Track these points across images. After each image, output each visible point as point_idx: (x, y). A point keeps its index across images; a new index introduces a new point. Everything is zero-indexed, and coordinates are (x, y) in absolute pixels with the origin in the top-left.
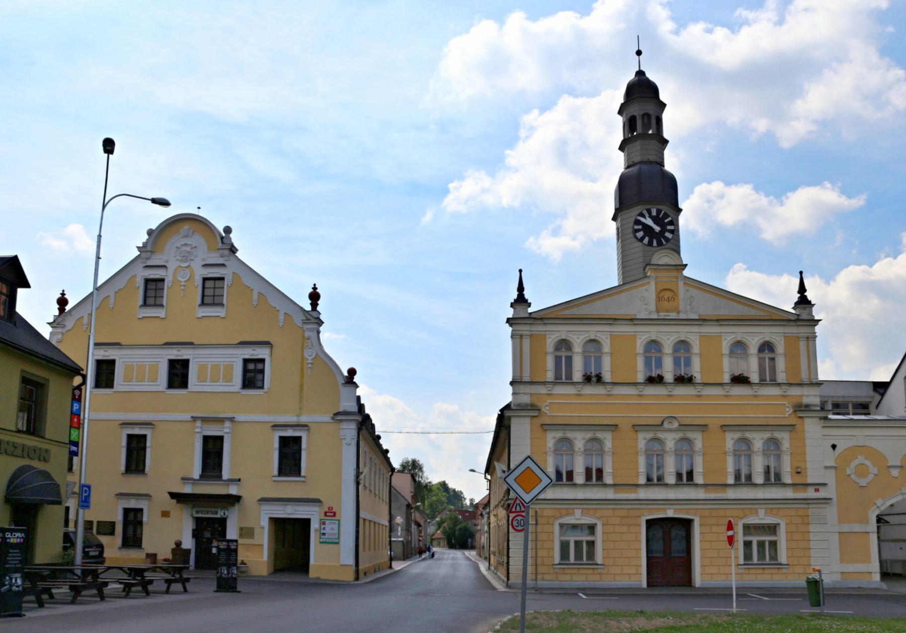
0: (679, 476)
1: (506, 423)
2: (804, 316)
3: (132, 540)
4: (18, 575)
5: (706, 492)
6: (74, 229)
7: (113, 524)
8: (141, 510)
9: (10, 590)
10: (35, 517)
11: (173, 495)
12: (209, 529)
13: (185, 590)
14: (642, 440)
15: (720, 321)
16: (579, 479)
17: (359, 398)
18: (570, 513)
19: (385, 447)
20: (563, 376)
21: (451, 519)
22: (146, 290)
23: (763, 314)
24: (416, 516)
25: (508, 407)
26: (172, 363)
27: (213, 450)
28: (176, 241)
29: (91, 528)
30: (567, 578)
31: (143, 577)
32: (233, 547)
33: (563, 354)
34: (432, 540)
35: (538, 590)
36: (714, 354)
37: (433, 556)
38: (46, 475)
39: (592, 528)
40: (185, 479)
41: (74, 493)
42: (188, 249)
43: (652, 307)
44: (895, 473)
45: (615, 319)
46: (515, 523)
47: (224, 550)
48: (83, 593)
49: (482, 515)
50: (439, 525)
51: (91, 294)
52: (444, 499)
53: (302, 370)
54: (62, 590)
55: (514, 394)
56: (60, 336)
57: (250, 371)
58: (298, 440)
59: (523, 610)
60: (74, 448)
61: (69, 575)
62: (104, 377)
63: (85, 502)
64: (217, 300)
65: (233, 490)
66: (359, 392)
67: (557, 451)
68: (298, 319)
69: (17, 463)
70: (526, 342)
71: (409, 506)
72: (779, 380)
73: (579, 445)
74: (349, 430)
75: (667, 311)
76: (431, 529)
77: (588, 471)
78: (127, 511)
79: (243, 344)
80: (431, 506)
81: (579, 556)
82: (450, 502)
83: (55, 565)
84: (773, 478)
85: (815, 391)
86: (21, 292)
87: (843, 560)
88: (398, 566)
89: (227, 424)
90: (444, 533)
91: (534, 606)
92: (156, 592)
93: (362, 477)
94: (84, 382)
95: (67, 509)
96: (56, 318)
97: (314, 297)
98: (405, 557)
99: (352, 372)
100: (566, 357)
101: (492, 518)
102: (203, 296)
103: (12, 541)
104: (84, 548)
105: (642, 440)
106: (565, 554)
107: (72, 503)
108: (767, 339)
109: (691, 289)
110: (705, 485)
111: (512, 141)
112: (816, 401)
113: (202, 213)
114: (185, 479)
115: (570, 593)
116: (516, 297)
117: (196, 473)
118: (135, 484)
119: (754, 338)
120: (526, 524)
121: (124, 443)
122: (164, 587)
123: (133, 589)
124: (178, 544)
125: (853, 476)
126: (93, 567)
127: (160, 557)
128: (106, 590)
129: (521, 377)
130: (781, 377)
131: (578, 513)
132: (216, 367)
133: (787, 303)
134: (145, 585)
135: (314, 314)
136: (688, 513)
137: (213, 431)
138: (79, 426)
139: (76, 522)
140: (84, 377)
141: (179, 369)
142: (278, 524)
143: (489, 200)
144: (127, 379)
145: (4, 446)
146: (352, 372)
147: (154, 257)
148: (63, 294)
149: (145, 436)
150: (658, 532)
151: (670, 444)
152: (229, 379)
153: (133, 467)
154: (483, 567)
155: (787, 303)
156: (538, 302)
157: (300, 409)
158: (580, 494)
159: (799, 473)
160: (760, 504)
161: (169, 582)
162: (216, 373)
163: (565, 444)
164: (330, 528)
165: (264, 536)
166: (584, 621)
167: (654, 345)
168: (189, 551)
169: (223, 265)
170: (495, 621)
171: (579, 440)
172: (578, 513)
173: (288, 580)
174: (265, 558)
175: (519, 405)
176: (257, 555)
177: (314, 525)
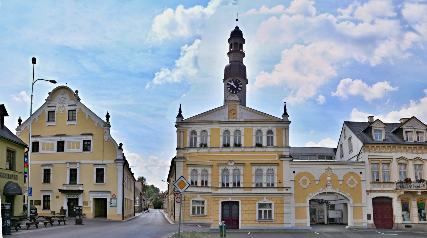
0: (235, 184)
1: (174, 163)
2: (285, 120)
3: (47, 207)
4: (9, 220)
5: (244, 191)
6: (23, 93)
7: (40, 201)
8: (49, 196)
9: (6, 226)
10: (14, 199)
11: (60, 190)
12: (73, 202)
13: (65, 224)
14: (221, 169)
15: (252, 122)
16: (199, 184)
17: (123, 154)
18: (196, 197)
19: (132, 172)
20: (193, 145)
21: (155, 198)
22: (49, 115)
23: (269, 119)
24: (143, 197)
25: (175, 158)
26: (59, 142)
27: (73, 174)
28: (59, 96)
29: (33, 203)
30: (194, 220)
31: (51, 220)
32: (81, 209)
33: (270, 135)
34: (149, 206)
35: (185, 224)
36: (248, 135)
37: (149, 211)
38: (17, 184)
39: (203, 202)
40: (64, 185)
41: (26, 191)
42: (63, 99)
43: (227, 117)
44: (317, 183)
45: (212, 122)
46: (177, 200)
47: (78, 210)
48: (31, 226)
49: (166, 197)
50: (151, 200)
51: (30, 118)
52: (153, 191)
53: (104, 144)
54: (23, 225)
55: (177, 153)
56: (19, 134)
57: (86, 145)
58: (102, 170)
59: (179, 231)
60: (26, 175)
61: (26, 220)
62: (35, 148)
63: (30, 194)
64: (74, 118)
65: (80, 188)
66: (123, 152)
67: (192, 174)
68: (102, 125)
69: (5, 181)
70: (182, 134)
71: (141, 193)
72: (274, 146)
73: (200, 172)
74: (120, 166)
75: (232, 118)
76: (148, 202)
77: (202, 182)
78: (44, 197)
79: (83, 134)
80: (148, 193)
81: (198, 212)
82: (155, 192)
83: (21, 216)
84: (271, 186)
85: (288, 150)
86: (5, 118)
87: (296, 218)
88: (137, 215)
89: (78, 164)
90: (153, 203)
91: (183, 229)
92: (55, 225)
93: (124, 183)
94: (28, 150)
95: (24, 196)
96: (18, 127)
97: (108, 116)
98: (139, 212)
99: (121, 145)
100: (195, 137)
101: (169, 198)
102: (69, 117)
103: (6, 208)
104: (30, 210)
105: (221, 169)
106: (260, 216)
107: (26, 194)
108: (270, 129)
109: (242, 110)
110: (244, 188)
111: (178, 57)
112: (288, 154)
113: (68, 86)
114: (64, 185)
115: (196, 225)
116: (178, 114)
117: (68, 182)
118: (47, 187)
119: (265, 128)
120: (181, 200)
121: (43, 172)
122: (58, 223)
123: (48, 224)
124: (62, 208)
125: (301, 184)
126: (34, 217)
127: (56, 213)
128: (38, 225)
129: (180, 147)
130: (275, 144)
131: (199, 196)
132: (74, 143)
133: (279, 115)
134: (52, 222)
135: (108, 123)
136: (237, 199)
137: (73, 167)
138: (27, 166)
139: (27, 201)
140: (28, 148)
141: (61, 145)
142: (96, 200)
143: (169, 79)
144: (43, 149)
145: (2, 175)
146: (121, 145)
147: (51, 103)
148: (20, 118)
149: (50, 169)
150: (227, 207)
151: (231, 171)
152: (78, 148)
153: (46, 181)
154: (166, 215)
155: (279, 115)
156: (186, 116)
157: (103, 158)
158: (199, 190)
159: (280, 183)
160: (266, 196)
161: (59, 221)
162: (73, 146)
163: (195, 172)
164: (114, 201)
165: (91, 205)
166: (200, 235)
167: (227, 132)
168: (66, 210)
169: (75, 105)
170: (170, 234)
171: (200, 170)
172: (199, 196)
173: (100, 220)
174: (92, 212)
175: (179, 157)
176: (89, 211)
177: (108, 201)
